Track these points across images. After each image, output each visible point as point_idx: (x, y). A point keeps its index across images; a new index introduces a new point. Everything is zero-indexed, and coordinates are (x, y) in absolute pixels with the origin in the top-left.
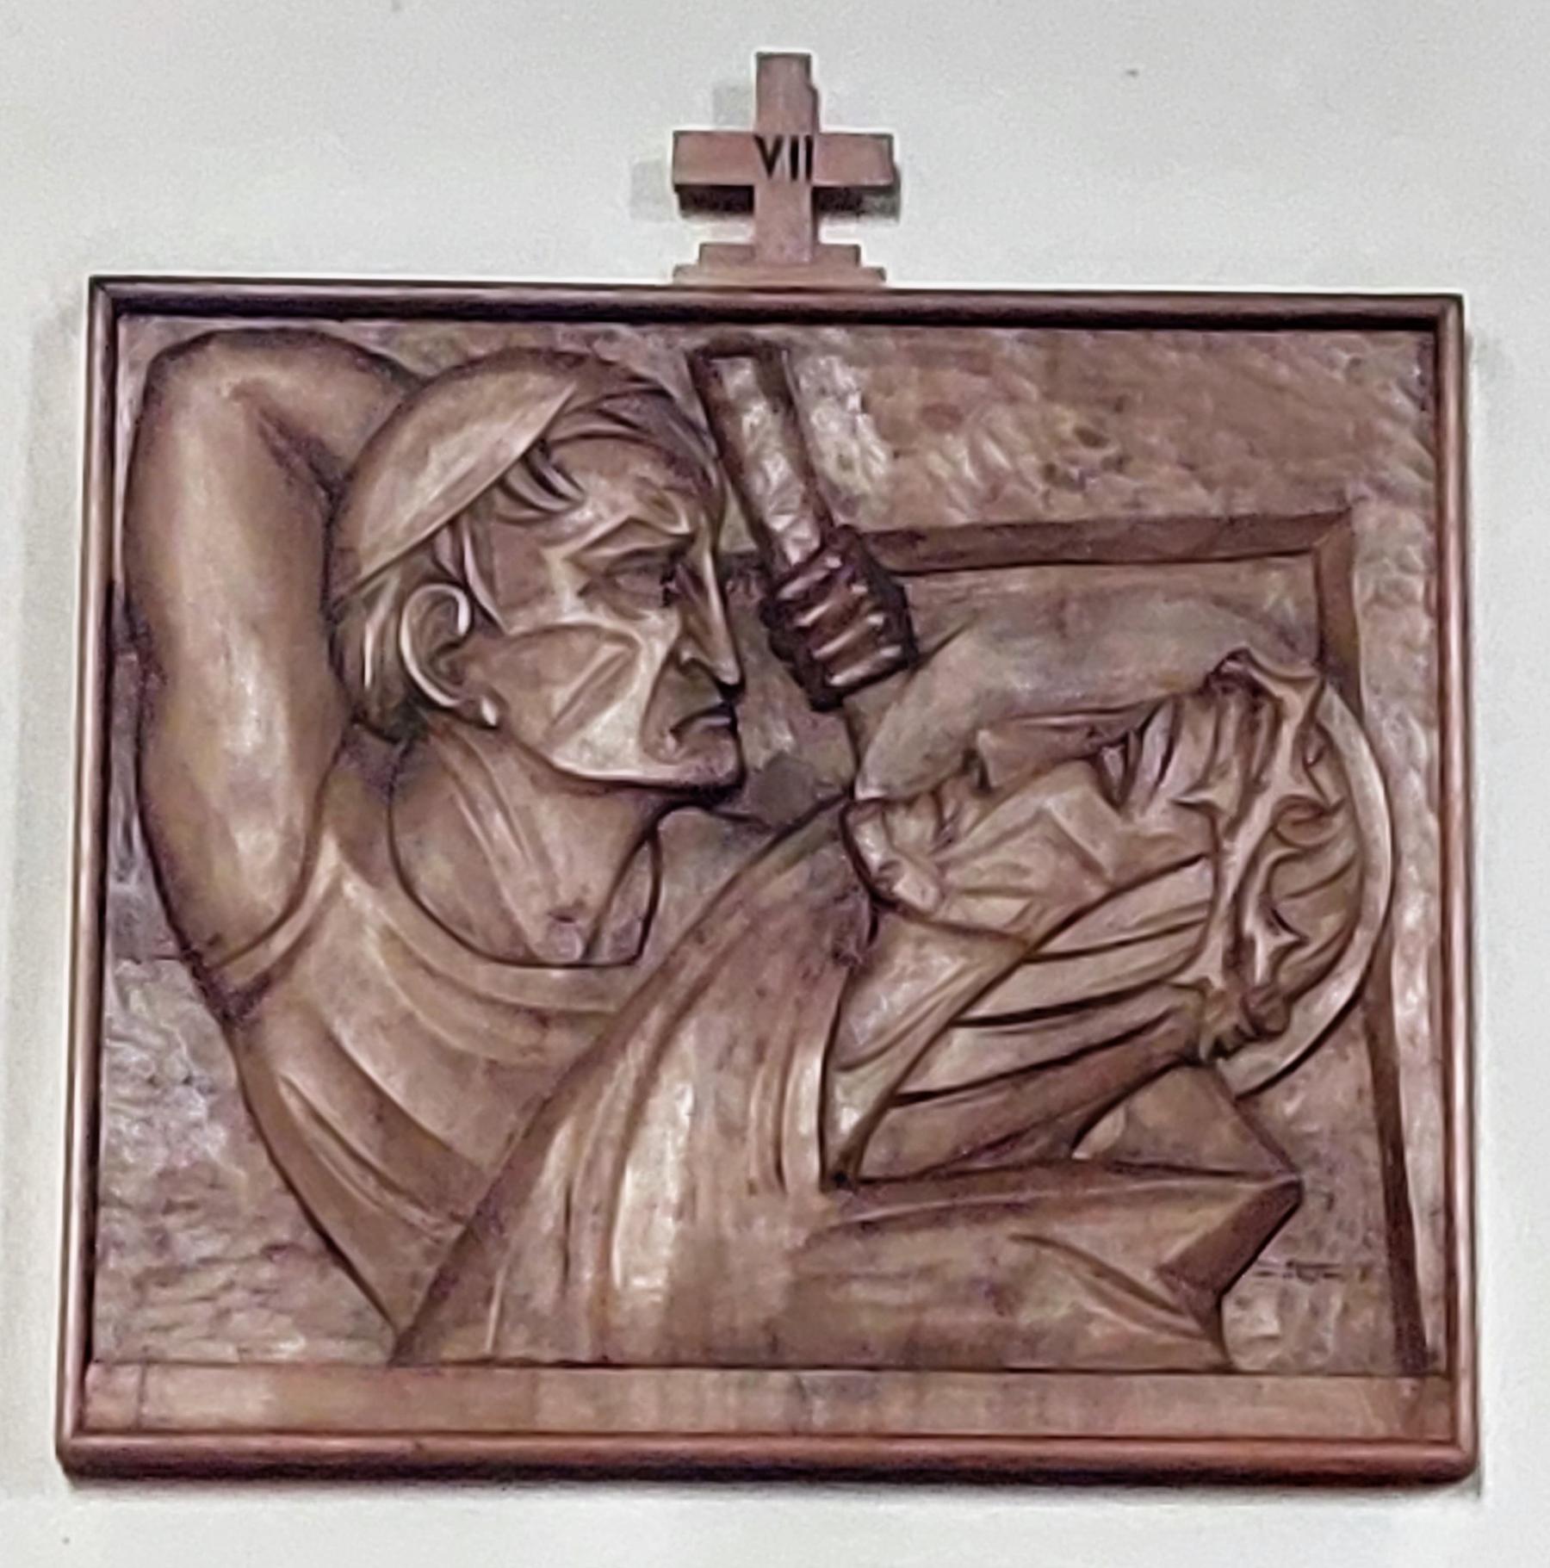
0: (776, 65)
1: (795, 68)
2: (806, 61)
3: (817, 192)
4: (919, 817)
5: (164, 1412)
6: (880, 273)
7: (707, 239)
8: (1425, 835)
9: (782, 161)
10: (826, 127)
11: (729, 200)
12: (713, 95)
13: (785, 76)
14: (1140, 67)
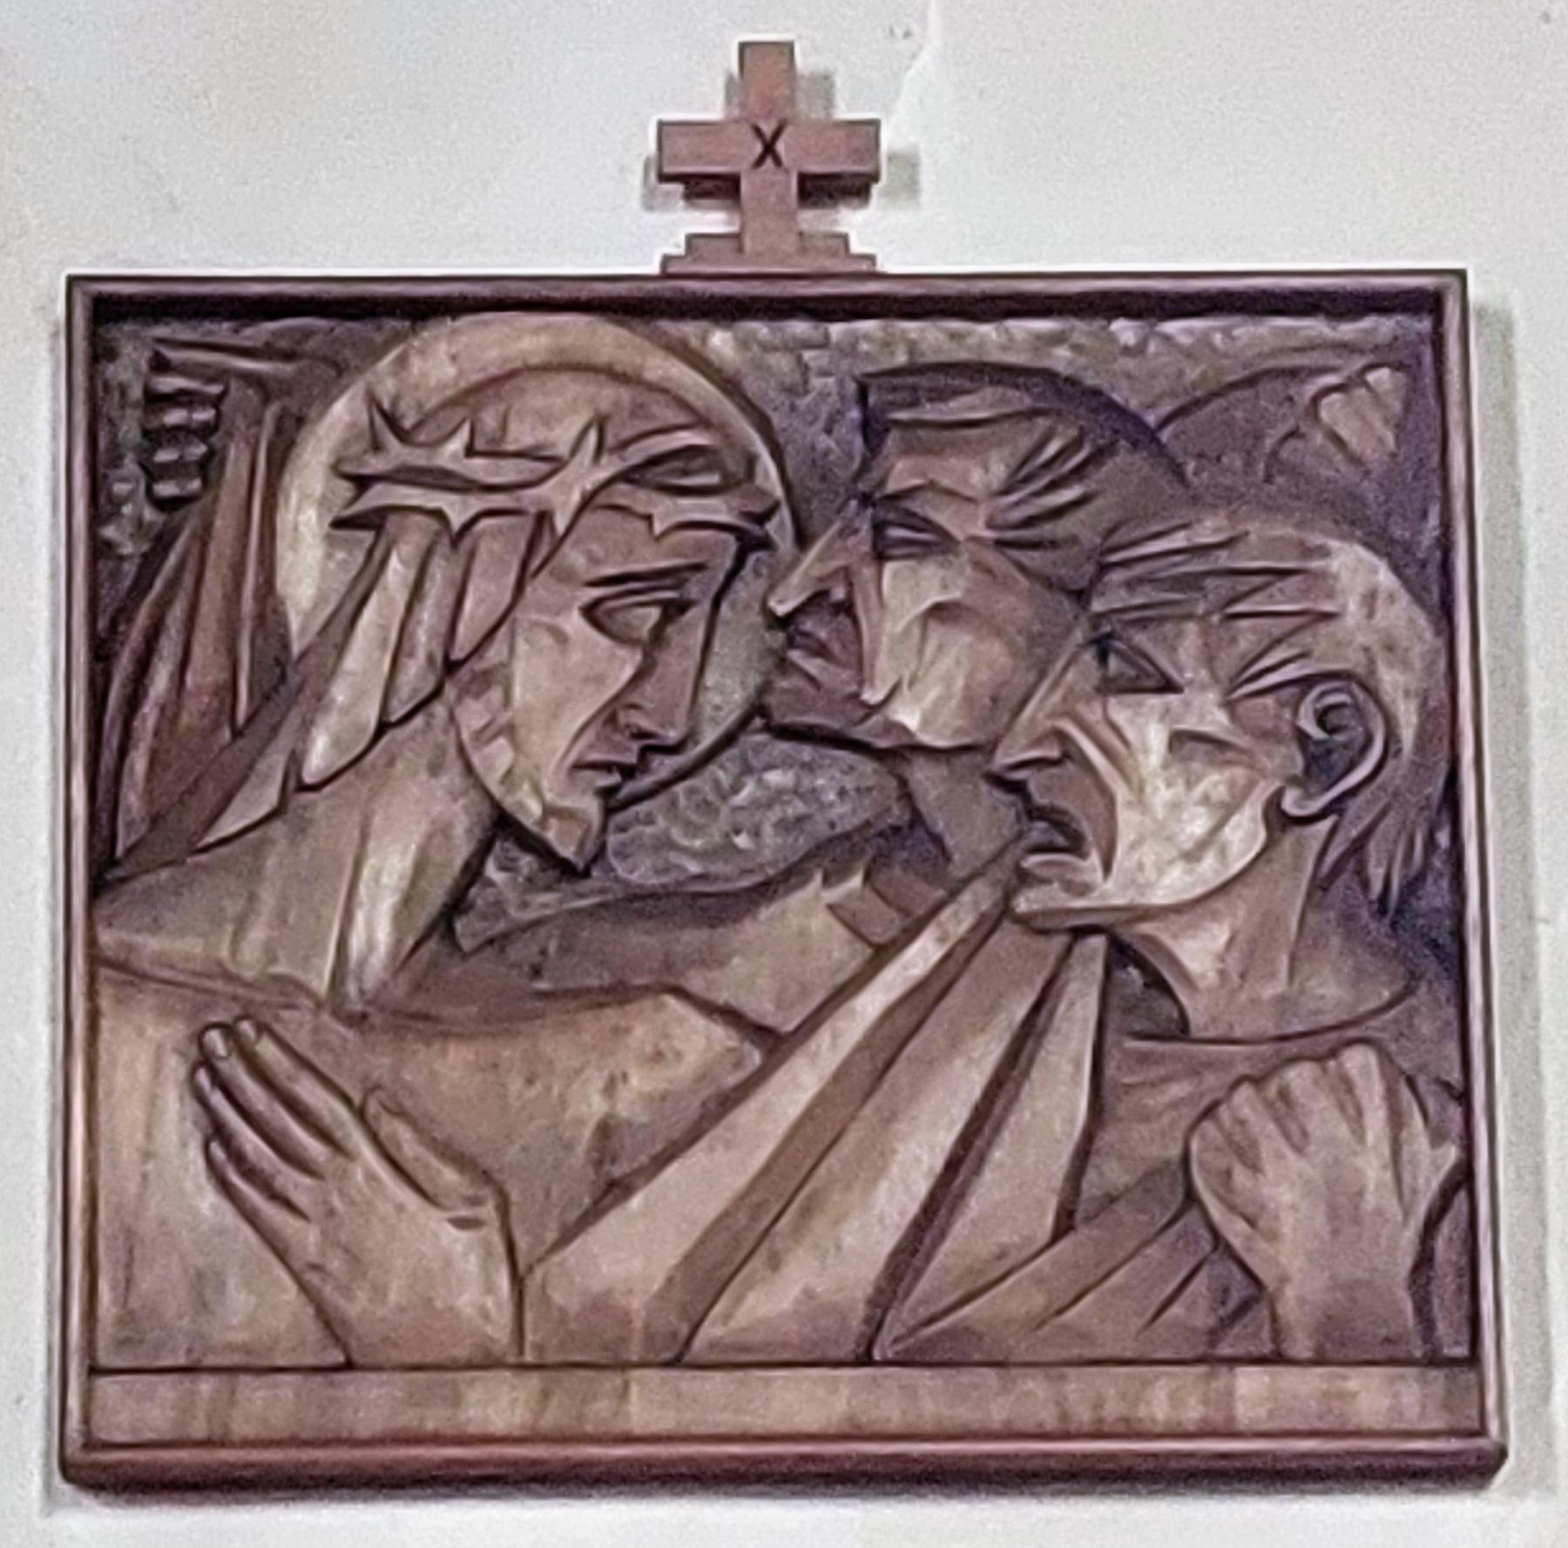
2: (787, 48)
9: (778, 150)
13: (765, 64)
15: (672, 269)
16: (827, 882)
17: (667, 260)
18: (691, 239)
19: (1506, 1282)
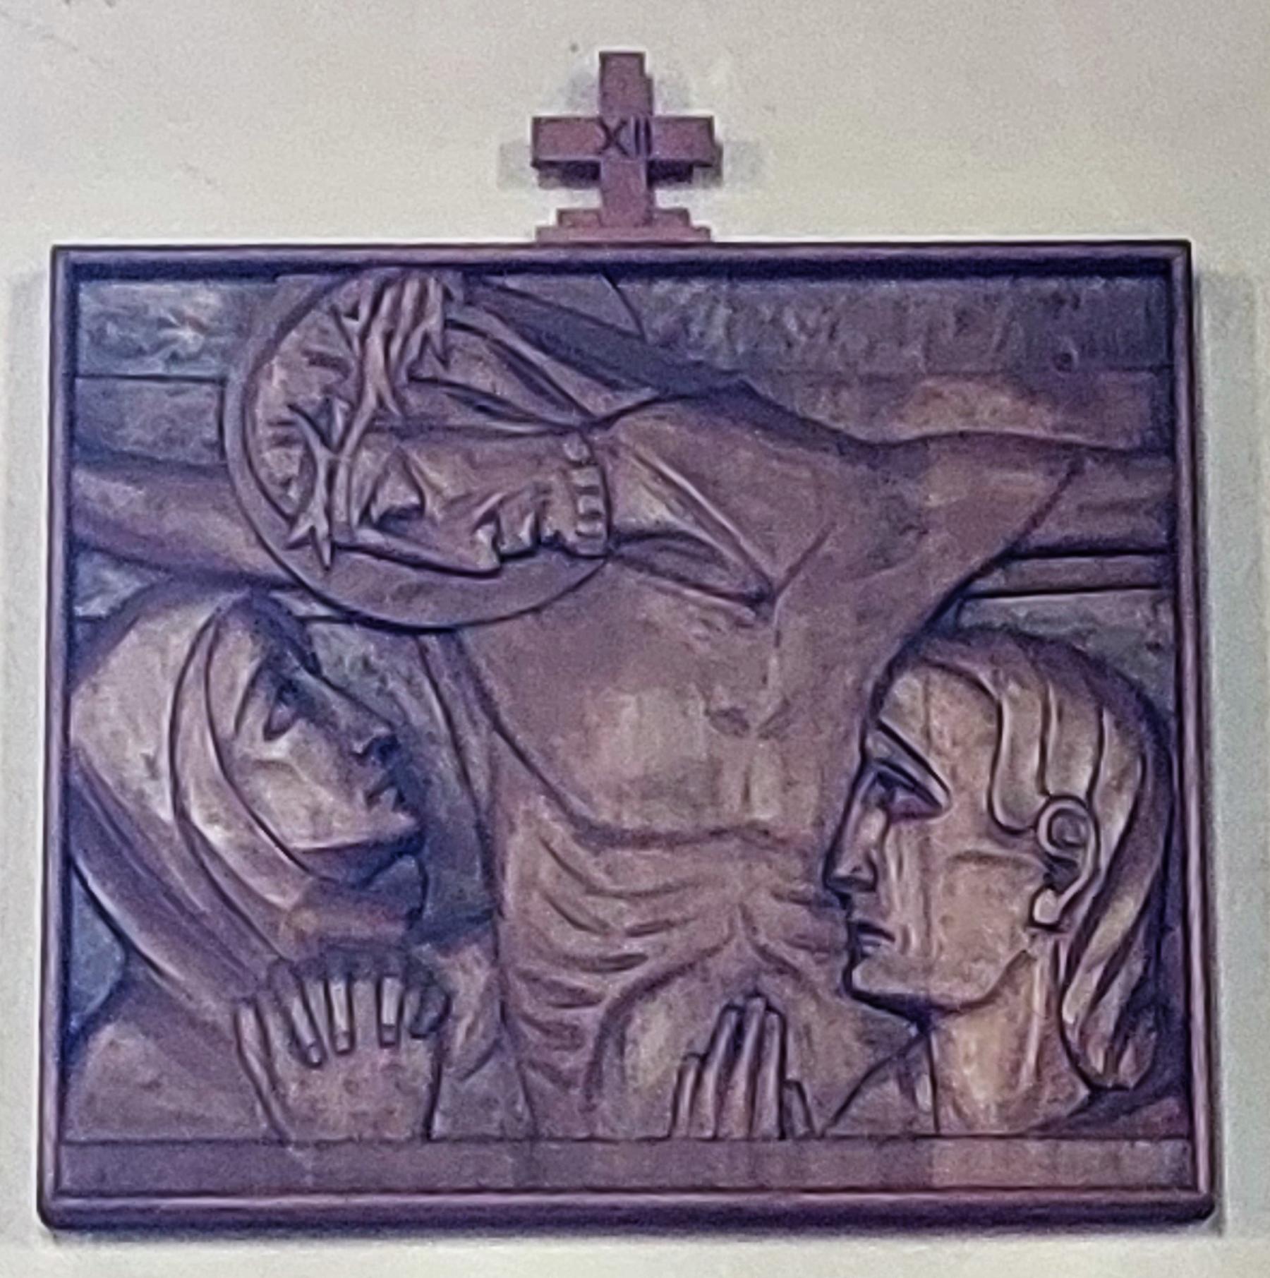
1: (636, 61)
2: (639, 57)
3: (651, 165)
4: (255, 644)
6: (707, 231)
9: (627, 139)
11: (580, 173)
13: (622, 72)
14: (565, 44)
17: (540, 231)
18: (562, 214)
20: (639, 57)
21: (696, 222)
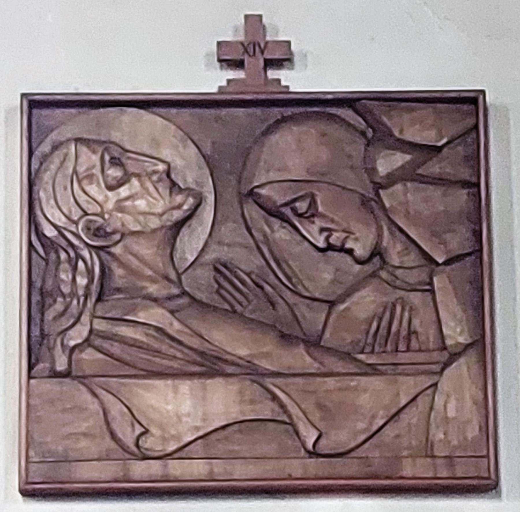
0: (250, 18)
2: (260, 16)
5: (200, 381)
7: (231, 77)
8: (448, 325)
9: (255, 50)
10: (268, 38)
11: (239, 64)
12: (232, 31)
13: (254, 22)
15: (223, 90)
16: (147, 288)
18: (229, 81)
19: (499, 388)
20: (260, 16)
21: (283, 83)
